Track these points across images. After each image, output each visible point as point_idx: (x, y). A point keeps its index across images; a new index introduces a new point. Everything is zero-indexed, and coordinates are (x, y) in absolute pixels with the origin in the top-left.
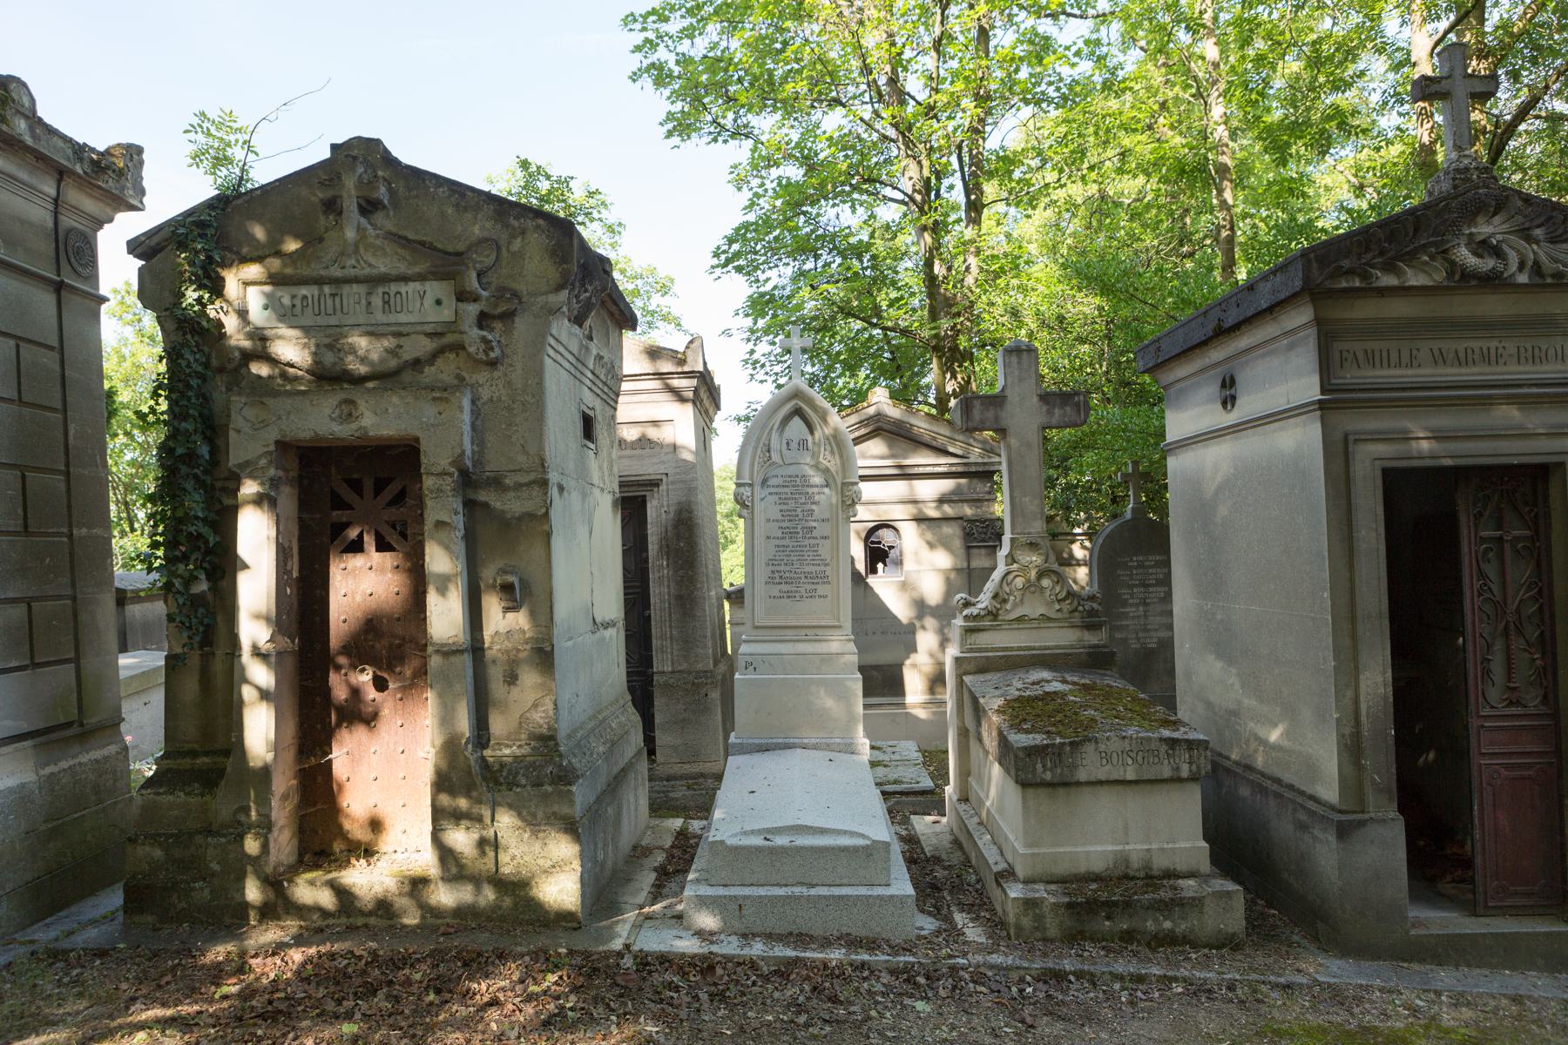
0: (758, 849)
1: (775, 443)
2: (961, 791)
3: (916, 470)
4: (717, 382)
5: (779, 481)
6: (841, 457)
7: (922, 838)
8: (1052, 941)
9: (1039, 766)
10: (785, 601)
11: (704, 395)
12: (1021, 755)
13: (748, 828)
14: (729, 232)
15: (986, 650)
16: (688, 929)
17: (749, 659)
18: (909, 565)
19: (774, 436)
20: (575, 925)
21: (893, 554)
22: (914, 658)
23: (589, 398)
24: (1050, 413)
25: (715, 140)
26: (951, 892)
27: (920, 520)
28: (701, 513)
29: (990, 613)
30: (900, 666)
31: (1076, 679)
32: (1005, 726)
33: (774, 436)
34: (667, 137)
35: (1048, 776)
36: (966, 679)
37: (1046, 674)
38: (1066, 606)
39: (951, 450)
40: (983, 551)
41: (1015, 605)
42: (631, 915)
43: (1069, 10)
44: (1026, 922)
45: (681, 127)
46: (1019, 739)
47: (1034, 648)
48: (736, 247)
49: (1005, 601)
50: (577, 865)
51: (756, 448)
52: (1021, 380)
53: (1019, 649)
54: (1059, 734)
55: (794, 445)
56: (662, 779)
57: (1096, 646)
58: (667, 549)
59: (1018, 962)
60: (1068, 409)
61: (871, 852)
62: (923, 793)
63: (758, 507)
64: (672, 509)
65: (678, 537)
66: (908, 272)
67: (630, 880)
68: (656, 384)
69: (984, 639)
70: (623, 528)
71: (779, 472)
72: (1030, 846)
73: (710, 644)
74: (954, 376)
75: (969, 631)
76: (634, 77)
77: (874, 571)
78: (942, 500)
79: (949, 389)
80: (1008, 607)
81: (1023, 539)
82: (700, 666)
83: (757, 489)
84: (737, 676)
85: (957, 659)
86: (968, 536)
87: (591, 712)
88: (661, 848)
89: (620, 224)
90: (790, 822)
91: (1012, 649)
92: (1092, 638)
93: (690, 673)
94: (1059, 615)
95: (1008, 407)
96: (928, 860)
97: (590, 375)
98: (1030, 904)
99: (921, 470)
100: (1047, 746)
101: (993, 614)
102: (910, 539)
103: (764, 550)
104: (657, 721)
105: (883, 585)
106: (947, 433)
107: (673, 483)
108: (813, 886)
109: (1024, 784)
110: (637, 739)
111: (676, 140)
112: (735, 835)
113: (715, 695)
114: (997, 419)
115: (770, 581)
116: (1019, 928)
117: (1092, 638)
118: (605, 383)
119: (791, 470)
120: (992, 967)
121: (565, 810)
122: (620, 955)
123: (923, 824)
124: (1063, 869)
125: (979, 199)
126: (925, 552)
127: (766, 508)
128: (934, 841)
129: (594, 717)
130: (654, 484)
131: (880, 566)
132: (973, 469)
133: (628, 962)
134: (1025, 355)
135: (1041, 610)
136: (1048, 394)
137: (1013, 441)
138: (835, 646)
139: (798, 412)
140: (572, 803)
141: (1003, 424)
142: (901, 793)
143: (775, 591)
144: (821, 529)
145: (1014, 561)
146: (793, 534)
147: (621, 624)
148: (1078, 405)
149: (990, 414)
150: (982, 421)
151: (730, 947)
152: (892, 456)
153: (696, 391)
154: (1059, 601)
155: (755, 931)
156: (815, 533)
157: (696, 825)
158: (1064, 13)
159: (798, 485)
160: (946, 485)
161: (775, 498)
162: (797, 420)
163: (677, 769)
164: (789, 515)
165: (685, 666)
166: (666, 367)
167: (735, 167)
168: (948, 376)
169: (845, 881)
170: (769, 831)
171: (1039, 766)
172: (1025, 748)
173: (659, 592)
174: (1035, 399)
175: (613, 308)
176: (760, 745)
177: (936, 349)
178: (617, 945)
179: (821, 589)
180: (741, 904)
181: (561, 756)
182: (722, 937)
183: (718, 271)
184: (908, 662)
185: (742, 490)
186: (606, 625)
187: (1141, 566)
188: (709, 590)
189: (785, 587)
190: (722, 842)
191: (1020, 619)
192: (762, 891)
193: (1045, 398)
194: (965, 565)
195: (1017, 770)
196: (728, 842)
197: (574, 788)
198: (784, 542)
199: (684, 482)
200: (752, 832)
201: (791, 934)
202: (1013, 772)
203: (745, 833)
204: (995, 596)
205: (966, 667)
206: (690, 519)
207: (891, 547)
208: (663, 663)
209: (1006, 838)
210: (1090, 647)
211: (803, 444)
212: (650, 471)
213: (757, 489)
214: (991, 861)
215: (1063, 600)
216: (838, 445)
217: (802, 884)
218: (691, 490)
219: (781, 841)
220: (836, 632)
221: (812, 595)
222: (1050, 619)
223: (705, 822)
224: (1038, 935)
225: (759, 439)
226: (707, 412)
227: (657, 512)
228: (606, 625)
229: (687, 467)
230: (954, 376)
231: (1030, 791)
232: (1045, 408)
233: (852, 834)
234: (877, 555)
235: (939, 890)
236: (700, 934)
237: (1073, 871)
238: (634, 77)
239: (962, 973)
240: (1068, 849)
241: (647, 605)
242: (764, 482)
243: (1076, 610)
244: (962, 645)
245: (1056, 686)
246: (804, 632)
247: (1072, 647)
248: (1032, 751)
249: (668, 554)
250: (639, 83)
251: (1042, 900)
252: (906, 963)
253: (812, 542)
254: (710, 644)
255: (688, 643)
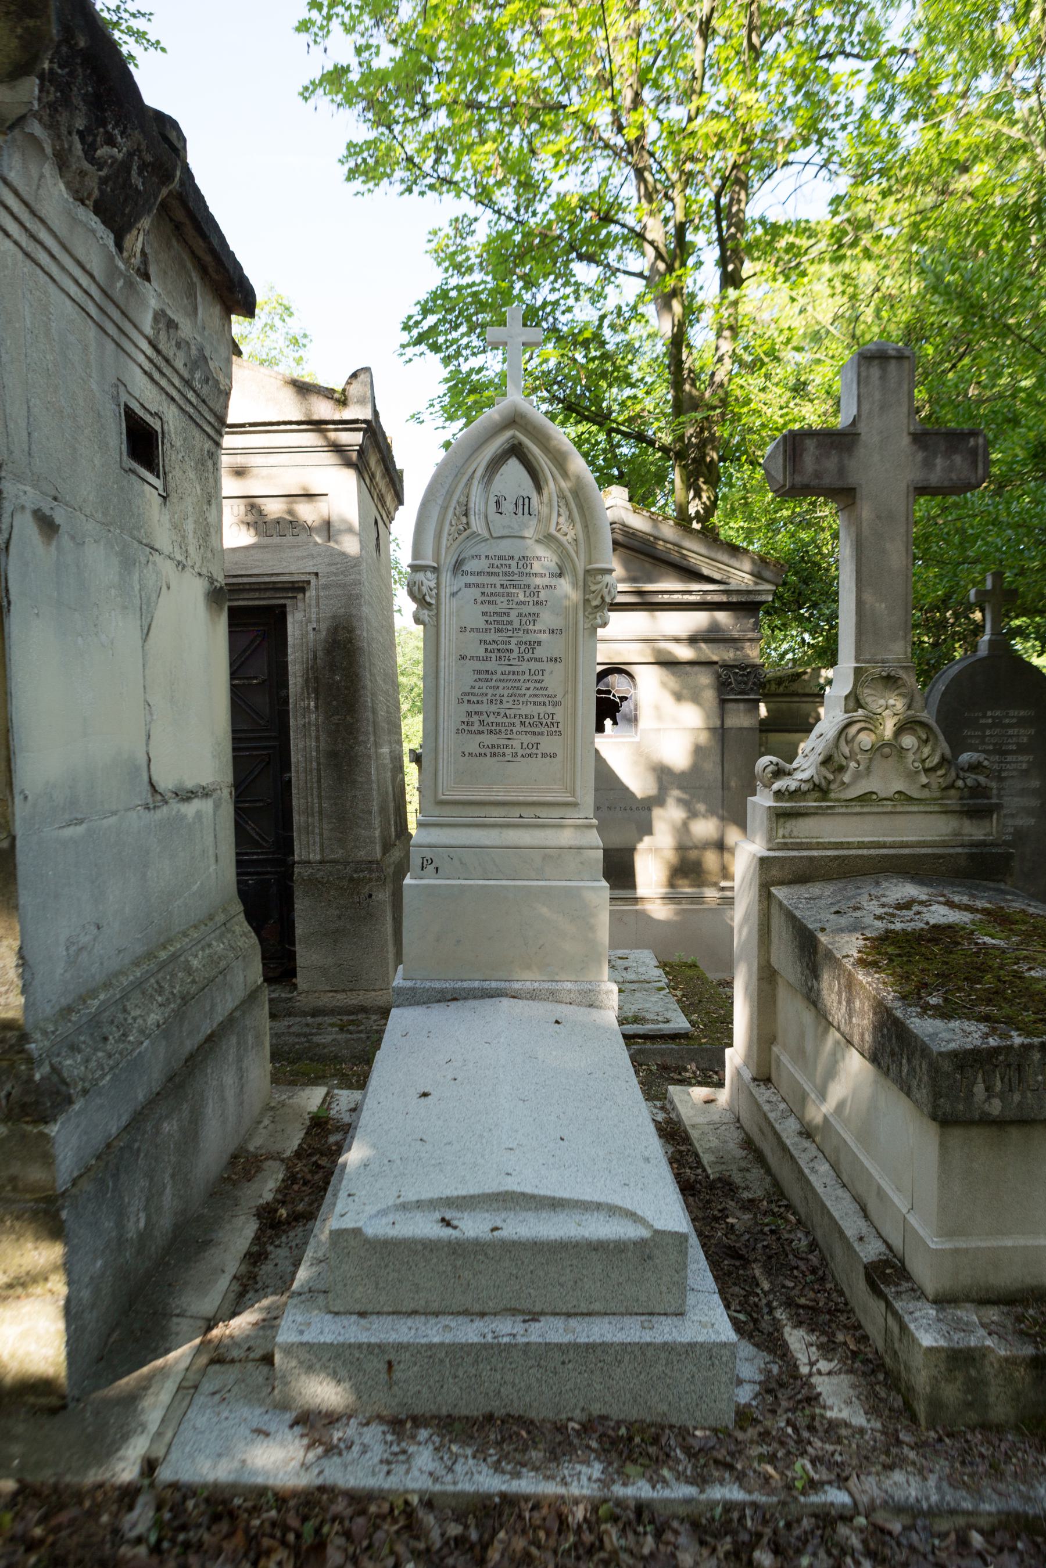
0: (430, 1246)
1: (476, 501)
2: (759, 1066)
3: (660, 598)
4: (399, 466)
5: (482, 565)
6: (586, 527)
7: (694, 1134)
8: (999, 1429)
9: (979, 1089)
10: (489, 761)
11: (373, 460)
12: (947, 1066)
13: (411, 1196)
14: (423, 296)
15: (809, 847)
16: (283, 1406)
17: (428, 853)
18: (645, 721)
19: (476, 489)
20: (54, 1401)
21: (625, 707)
22: (646, 842)
23: (146, 396)
24: (928, 464)
25: (409, 190)
26: (768, 1272)
27: (668, 663)
28: (367, 632)
29: (817, 787)
30: (631, 851)
31: (965, 900)
32: (889, 995)
33: (476, 489)
34: (348, 179)
35: (995, 1107)
36: (780, 892)
37: (910, 890)
38: (936, 780)
39: (706, 572)
40: (742, 706)
41: (857, 776)
42: (180, 1356)
43: (848, 49)
44: (951, 1393)
45: (367, 166)
46: (949, 1034)
47: (883, 845)
48: (431, 320)
49: (841, 769)
50: (59, 1286)
51: (445, 509)
52: (883, 408)
53: (861, 845)
54: (1010, 1021)
55: (508, 507)
56: (305, 1014)
57: (982, 844)
58: (315, 683)
59: (951, 1497)
60: (958, 459)
61: (649, 1251)
62: (675, 1037)
63: (447, 606)
64: (324, 626)
65: (332, 667)
66: (647, 362)
67: (208, 1243)
68: (310, 439)
69: (806, 829)
70: (231, 633)
71: (483, 549)
72: (949, 1233)
73: (376, 822)
74: (698, 495)
75: (780, 816)
76: (306, 93)
77: (600, 728)
78: (693, 640)
79: (692, 511)
80: (847, 778)
81: (876, 670)
82: (362, 855)
83: (446, 577)
84: (408, 881)
85: (763, 861)
86: (723, 686)
87: (139, 950)
88: (277, 1157)
89: (305, 336)
90: (491, 1186)
91: (848, 845)
92: (975, 831)
93: (346, 863)
94: (926, 794)
95: (861, 451)
96: (712, 1186)
97: (144, 345)
98: (959, 1360)
99: (666, 598)
100: (997, 1050)
101: (820, 789)
102: (649, 690)
103: (456, 678)
104: (299, 931)
105: (615, 747)
106: (703, 551)
107: (326, 587)
108: (534, 1317)
109: (945, 1121)
110: (251, 971)
111: (358, 184)
112: (384, 1212)
113: (383, 896)
114: (842, 471)
115: (465, 728)
116: (936, 1404)
117: (975, 831)
118: (188, 383)
119: (504, 548)
120: (900, 1509)
121: (36, 1174)
122: (128, 1495)
123: (691, 1099)
124: (1009, 1277)
125: (737, 271)
126: (668, 701)
127: (462, 608)
128: (714, 1143)
129: (150, 955)
130: (298, 588)
131: (608, 722)
132: (734, 599)
133: (140, 1519)
134: (893, 366)
135: (899, 785)
136: (925, 433)
137: (866, 511)
138: (566, 837)
139: (516, 451)
140: (48, 1159)
141: (852, 481)
142: (646, 1037)
143: (473, 744)
144: (550, 645)
145: (859, 705)
146: (503, 653)
147: (226, 794)
148: (974, 452)
149: (831, 463)
150: (818, 475)
151: (363, 1467)
152: (633, 580)
153: (361, 452)
154: (927, 771)
155: (418, 1411)
156: (539, 652)
157: (345, 1098)
158: (843, 52)
159: (513, 571)
160: (697, 620)
161: (475, 592)
162: (513, 465)
163: (326, 1000)
164: (497, 622)
165: (339, 854)
166: (324, 410)
167: (435, 233)
168: (691, 494)
169: (597, 1307)
170: (450, 1202)
171: (979, 1089)
172: (954, 1054)
173: (304, 747)
174: (906, 441)
175: (199, 245)
176: (442, 991)
177: (680, 456)
178: (126, 1469)
179: (547, 744)
180: (389, 1360)
181: (30, 1060)
182: (351, 1430)
183: (411, 351)
184: (640, 846)
185: (420, 576)
186: (186, 795)
187: (997, 724)
188: (377, 745)
189: (488, 739)
190: (357, 1232)
191: (864, 799)
192: (433, 1332)
193: (921, 438)
194: (718, 723)
195: (936, 1095)
196: (370, 1231)
197: (53, 1130)
198: (489, 666)
199: (342, 586)
200: (419, 1205)
201: (490, 1418)
202: (923, 1094)
203: (404, 1207)
204: (827, 761)
205: (775, 872)
206: (350, 641)
207: (623, 699)
208: (307, 849)
209: (880, 1192)
210: (972, 845)
211: (523, 505)
212: (293, 569)
213: (446, 577)
214: (850, 1233)
215: (933, 769)
216: (581, 508)
217: (514, 1312)
218: (352, 598)
219: (473, 1226)
220: (568, 812)
221: (531, 752)
222: (910, 799)
223: (357, 1095)
224: (972, 1417)
225: (450, 493)
226: (381, 499)
227: (302, 629)
228: (186, 795)
229: (347, 564)
230: (698, 495)
231: (957, 1134)
232: (920, 456)
233: (613, 1210)
234: (608, 708)
235: (746, 1262)
236: (312, 1423)
237: (1030, 1281)
238: (306, 93)
239: (843, 1530)
240: (1021, 1241)
241: (286, 764)
242: (458, 566)
243: (952, 786)
244: (770, 840)
245: (940, 914)
246: (516, 811)
247: (944, 844)
248: (969, 1060)
249: (316, 691)
250: (312, 102)
251: (983, 1352)
252: (729, 1507)
253: (534, 666)
254: (376, 822)
255: (344, 820)
